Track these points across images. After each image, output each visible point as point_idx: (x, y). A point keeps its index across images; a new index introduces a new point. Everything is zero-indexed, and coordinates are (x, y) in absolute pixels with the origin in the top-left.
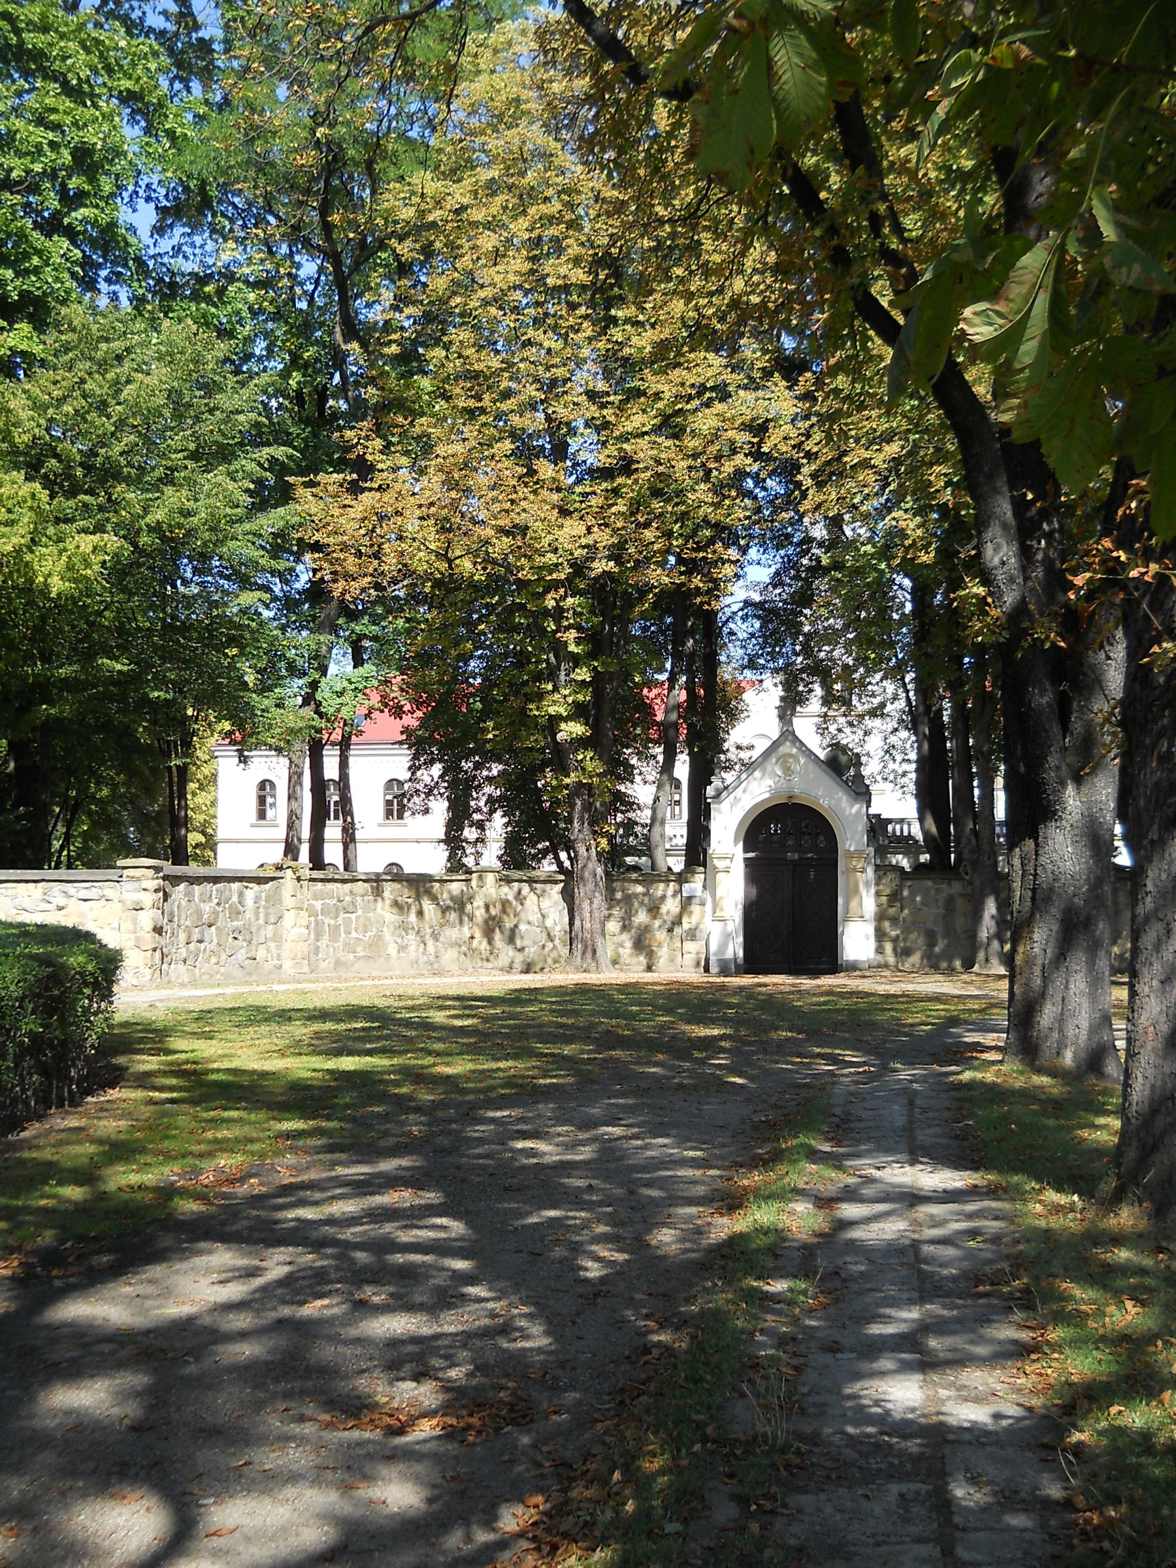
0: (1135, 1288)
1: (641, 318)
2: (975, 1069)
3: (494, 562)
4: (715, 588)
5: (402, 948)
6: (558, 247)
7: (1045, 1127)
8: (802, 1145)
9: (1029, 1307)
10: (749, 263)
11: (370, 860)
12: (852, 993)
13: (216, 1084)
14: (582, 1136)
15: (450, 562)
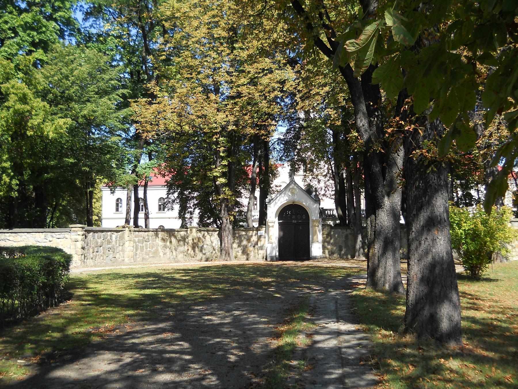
0: (412, 361)
1: (244, 47)
2: (357, 291)
3: (195, 127)
4: (269, 134)
5: (165, 254)
6: (217, 25)
7: (380, 310)
8: (300, 316)
9: (378, 368)
10: (278, 29)
11: (154, 224)
12: (315, 267)
13: (104, 299)
14: (227, 314)
15: (181, 127)
